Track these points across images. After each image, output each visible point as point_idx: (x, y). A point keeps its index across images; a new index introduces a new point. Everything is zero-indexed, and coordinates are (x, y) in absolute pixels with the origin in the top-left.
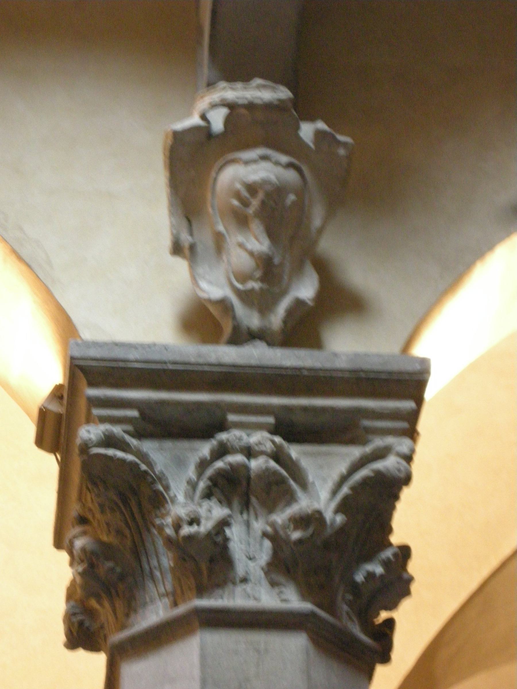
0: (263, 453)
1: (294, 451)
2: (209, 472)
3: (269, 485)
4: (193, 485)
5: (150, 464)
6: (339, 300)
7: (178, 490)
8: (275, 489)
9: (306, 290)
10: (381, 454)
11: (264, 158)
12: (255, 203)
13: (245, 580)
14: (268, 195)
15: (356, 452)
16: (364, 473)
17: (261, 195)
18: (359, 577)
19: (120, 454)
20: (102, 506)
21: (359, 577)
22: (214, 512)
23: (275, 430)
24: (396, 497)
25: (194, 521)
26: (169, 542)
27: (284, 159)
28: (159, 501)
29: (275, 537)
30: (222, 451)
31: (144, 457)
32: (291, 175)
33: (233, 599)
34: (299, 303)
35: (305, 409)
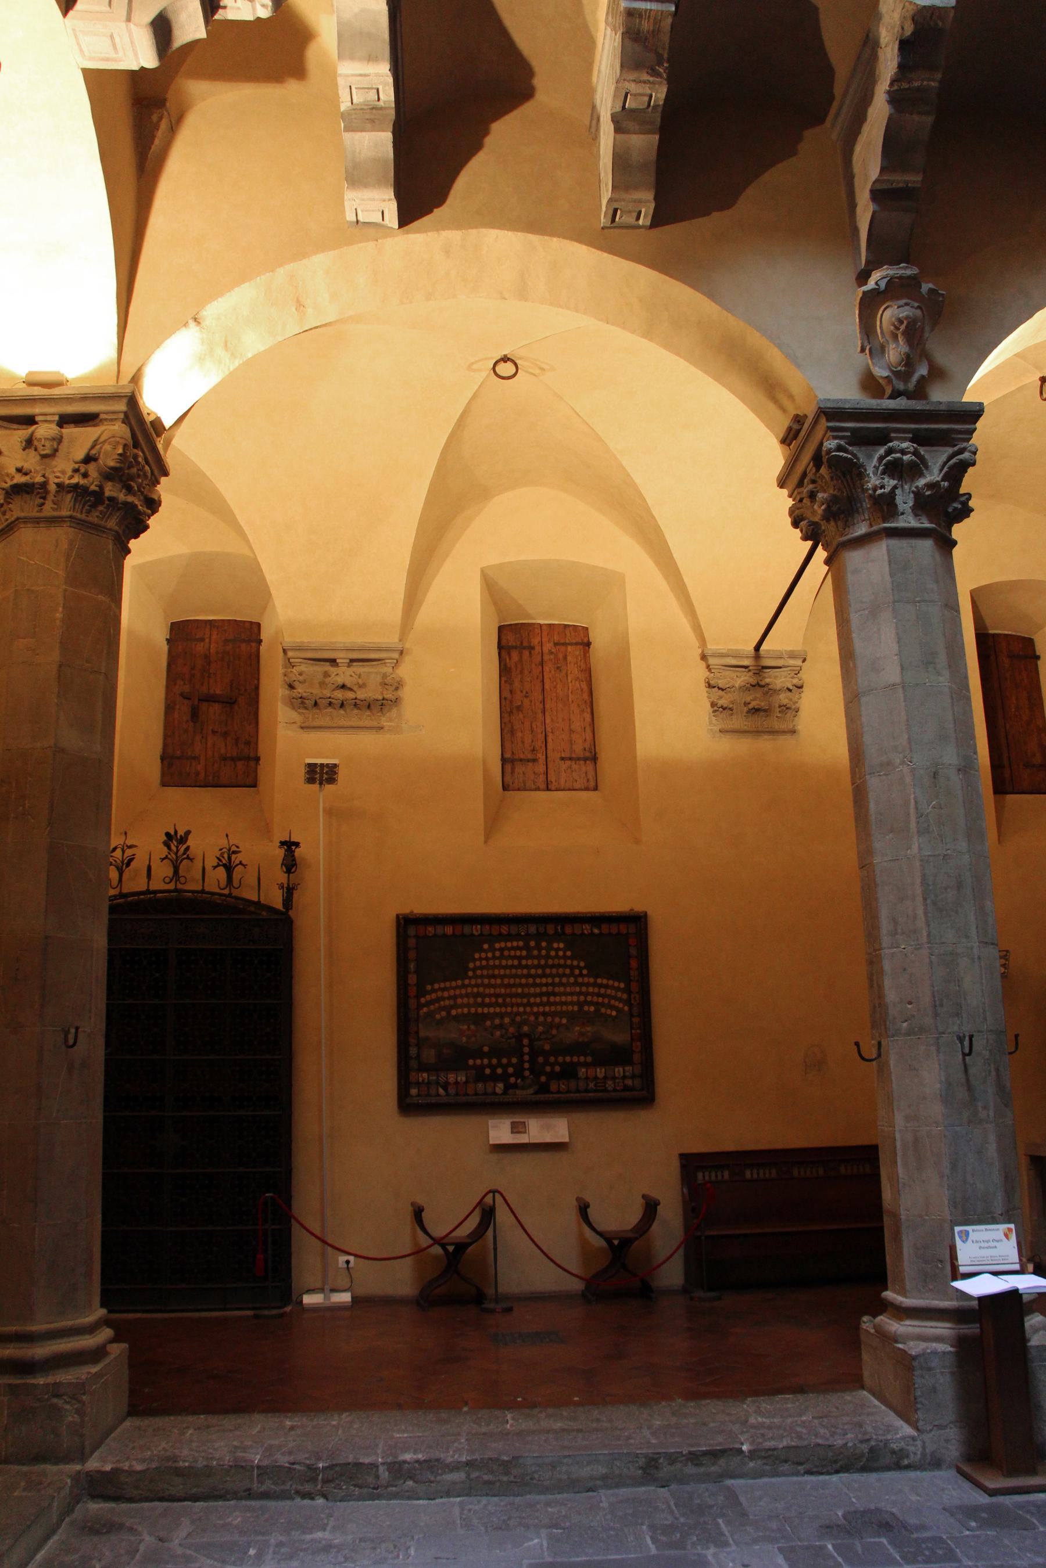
0: (909, 453)
1: (922, 451)
2: (884, 462)
4: (876, 468)
5: (858, 459)
6: (937, 373)
7: (870, 471)
8: (916, 469)
9: (923, 370)
10: (962, 451)
11: (907, 304)
12: (903, 327)
13: (903, 514)
14: (909, 323)
15: (950, 450)
18: (950, 510)
19: (845, 455)
20: (832, 478)
21: (950, 510)
23: (912, 440)
25: (882, 487)
26: (870, 496)
27: (916, 304)
29: (918, 494)
32: (918, 312)
33: (901, 523)
34: (923, 377)
35: (926, 430)
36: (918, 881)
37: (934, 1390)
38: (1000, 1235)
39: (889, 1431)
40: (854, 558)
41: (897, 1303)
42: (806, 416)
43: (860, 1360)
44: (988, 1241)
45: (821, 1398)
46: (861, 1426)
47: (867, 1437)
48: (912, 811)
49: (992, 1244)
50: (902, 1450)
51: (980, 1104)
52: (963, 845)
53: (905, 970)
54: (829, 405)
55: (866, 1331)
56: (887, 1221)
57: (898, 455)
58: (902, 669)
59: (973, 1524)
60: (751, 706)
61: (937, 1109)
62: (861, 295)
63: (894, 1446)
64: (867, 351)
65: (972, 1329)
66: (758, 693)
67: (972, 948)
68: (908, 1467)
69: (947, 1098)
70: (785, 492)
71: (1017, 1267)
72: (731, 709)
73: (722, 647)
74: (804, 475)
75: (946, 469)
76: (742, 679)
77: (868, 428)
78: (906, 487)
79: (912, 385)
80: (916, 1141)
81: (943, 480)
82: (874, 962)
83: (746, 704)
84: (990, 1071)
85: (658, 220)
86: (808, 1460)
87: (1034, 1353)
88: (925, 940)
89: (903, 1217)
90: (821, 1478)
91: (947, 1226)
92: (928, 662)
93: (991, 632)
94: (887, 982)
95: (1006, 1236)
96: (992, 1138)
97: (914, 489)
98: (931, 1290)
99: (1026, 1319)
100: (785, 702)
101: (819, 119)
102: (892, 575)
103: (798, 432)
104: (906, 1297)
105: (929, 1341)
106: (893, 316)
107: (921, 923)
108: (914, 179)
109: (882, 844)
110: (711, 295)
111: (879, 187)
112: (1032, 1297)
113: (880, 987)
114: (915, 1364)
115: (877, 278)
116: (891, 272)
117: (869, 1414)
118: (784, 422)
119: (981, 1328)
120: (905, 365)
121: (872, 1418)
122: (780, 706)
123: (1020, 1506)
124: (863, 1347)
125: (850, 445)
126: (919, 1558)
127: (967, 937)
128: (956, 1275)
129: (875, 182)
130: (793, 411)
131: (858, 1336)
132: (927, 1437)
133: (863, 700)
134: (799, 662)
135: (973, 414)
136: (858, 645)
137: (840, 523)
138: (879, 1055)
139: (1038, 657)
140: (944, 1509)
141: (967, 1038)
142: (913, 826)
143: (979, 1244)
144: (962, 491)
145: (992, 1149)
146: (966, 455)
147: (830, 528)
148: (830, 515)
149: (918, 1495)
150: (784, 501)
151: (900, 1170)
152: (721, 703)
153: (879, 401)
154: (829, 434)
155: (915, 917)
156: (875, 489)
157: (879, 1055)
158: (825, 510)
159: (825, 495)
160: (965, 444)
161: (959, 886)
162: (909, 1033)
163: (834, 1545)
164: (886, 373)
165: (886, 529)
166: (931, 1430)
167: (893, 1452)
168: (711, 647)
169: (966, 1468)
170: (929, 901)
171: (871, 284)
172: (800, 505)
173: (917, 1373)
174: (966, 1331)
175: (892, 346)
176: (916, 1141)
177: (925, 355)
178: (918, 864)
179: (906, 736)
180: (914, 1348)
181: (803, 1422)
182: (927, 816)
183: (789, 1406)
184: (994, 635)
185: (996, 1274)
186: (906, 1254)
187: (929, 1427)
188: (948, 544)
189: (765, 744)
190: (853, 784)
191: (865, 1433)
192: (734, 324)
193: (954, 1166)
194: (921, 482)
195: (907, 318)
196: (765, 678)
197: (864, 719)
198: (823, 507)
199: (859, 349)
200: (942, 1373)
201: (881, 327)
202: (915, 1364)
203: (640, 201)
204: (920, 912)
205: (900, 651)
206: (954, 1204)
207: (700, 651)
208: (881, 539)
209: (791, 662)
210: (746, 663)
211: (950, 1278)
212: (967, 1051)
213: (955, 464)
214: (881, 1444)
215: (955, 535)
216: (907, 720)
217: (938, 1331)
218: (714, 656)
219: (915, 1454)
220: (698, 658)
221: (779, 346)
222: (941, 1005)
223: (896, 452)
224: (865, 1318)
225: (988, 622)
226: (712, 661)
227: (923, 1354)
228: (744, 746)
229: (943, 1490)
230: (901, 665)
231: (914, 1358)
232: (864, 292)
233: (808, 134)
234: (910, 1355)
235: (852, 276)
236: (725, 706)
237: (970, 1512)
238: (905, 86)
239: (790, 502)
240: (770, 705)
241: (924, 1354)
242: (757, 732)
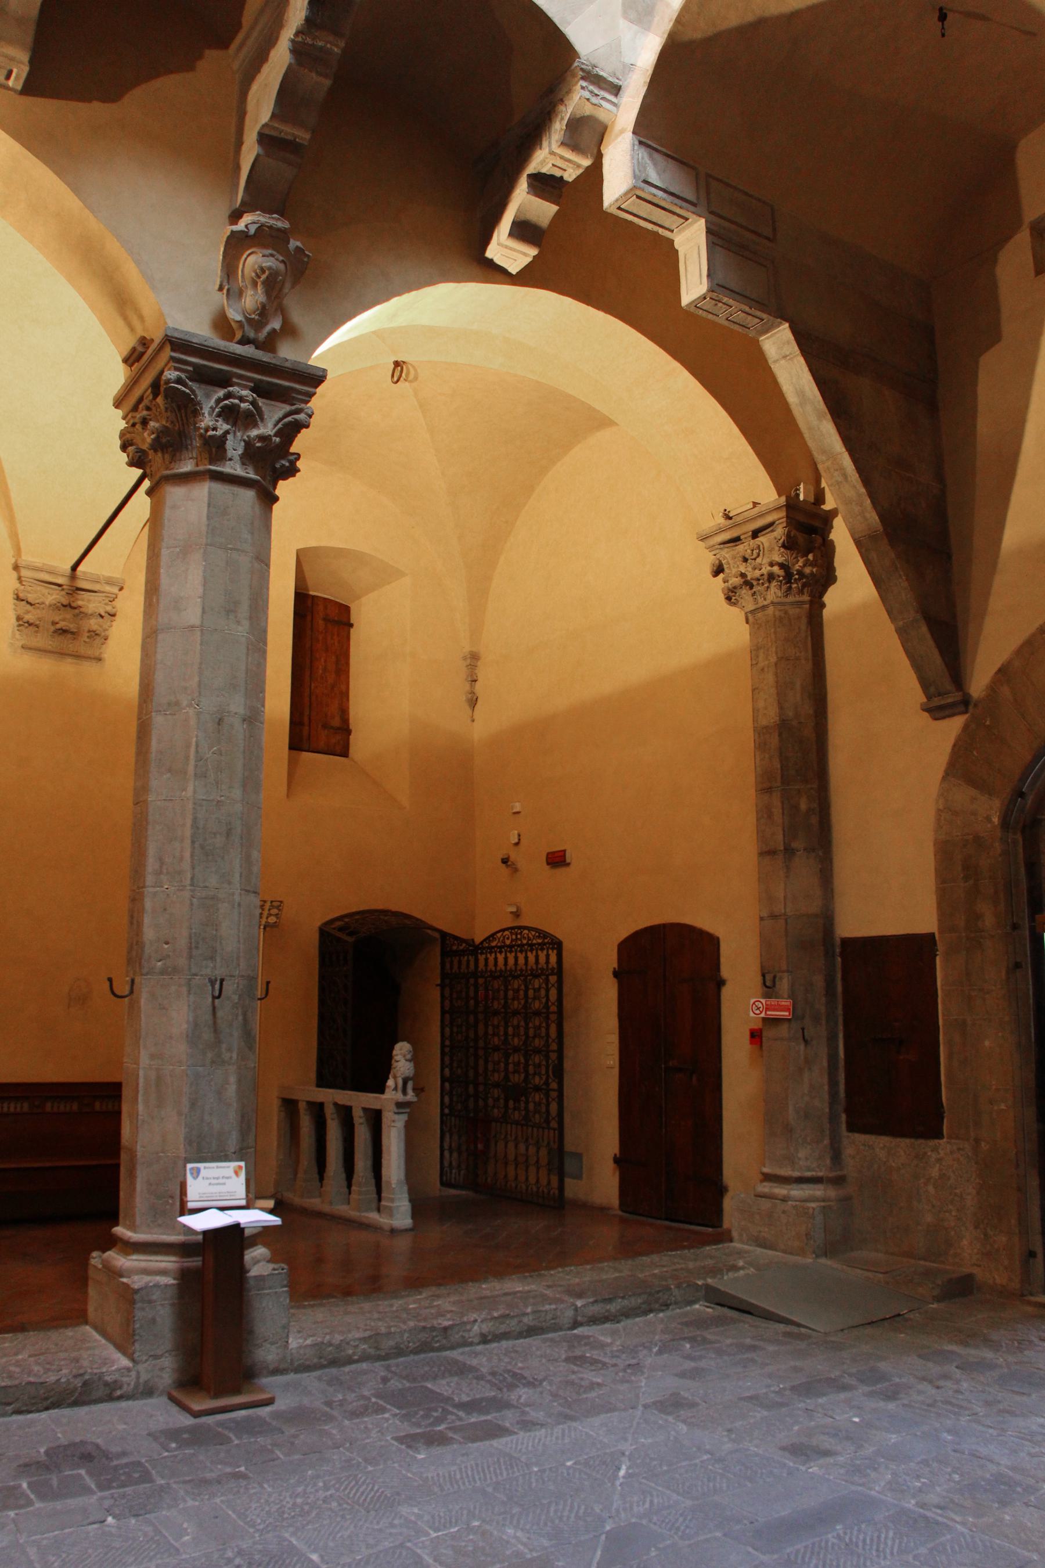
0: (247, 401)
1: (261, 402)
2: (221, 404)
3: (247, 416)
4: (213, 409)
5: (196, 395)
6: (289, 330)
7: (206, 411)
8: (251, 419)
9: (276, 324)
10: (298, 411)
11: (272, 255)
12: (264, 277)
13: (230, 460)
14: (270, 274)
15: (287, 408)
16: (289, 419)
17: (267, 273)
20: (166, 409)
21: (278, 466)
22: (223, 426)
23: (253, 390)
24: (299, 432)
25: (215, 429)
26: (201, 435)
27: (281, 258)
28: (196, 413)
29: (248, 444)
30: (229, 396)
31: (193, 391)
32: (282, 267)
33: (227, 468)
34: (274, 330)
35: (269, 383)
36: (189, 822)
37: (153, 1321)
38: (230, 1172)
39: (105, 1364)
40: (175, 493)
41: (126, 1238)
42: (152, 340)
43: (86, 1292)
44: (218, 1178)
45: (42, 1334)
46: (77, 1361)
47: (81, 1371)
48: (193, 749)
49: (221, 1181)
50: (115, 1381)
51: (224, 1046)
52: (237, 793)
53: (165, 910)
54: (176, 335)
55: (95, 1266)
56: (124, 1157)
57: (237, 401)
58: (204, 612)
59: (174, 1445)
60: (58, 626)
61: (181, 1049)
62: (228, 233)
63: (108, 1378)
64: (225, 291)
65: (195, 1262)
66: (69, 614)
67: (233, 894)
68: (120, 1398)
69: (193, 1038)
70: (120, 413)
71: (243, 1203)
72: (37, 626)
73: (38, 561)
74: (141, 399)
75: (280, 426)
76: (53, 597)
77: (212, 368)
78: (239, 434)
79: (262, 335)
80: (159, 1079)
81: (276, 435)
82: (136, 898)
83: (54, 623)
84: (237, 1015)
85: (29, 88)
86: (17, 1399)
87: (252, 1282)
88: (188, 882)
89: (139, 1154)
90: (30, 1416)
91: (181, 1163)
92: (230, 610)
93: (311, 593)
94: (147, 920)
95: (236, 1173)
96: (233, 1079)
97: (245, 438)
98: (160, 1225)
99: (246, 1252)
100: (95, 627)
101: (224, 44)
102: (209, 518)
103: (142, 354)
104: (135, 1232)
105: (150, 1274)
106: (256, 263)
107: (186, 865)
108: (303, 136)
109: (159, 783)
110: (76, 190)
111: (267, 131)
112: (255, 1231)
113: (140, 925)
114: (137, 1297)
115: (248, 221)
116: (263, 219)
117: (88, 1349)
118: (130, 342)
119: (203, 1261)
120: (260, 315)
121: (89, 1352)
122: (89, 631)
123: (220, 1424)
124: (90, 1283)
125: (191, 380)
126: (114, 1484)
127: (230, 883)
128: (184, 1211)
129: (263, 126)
130: (140, 332)
131: (86, 1271)
132: (141, 1367)
133: (160, 637)
134: (115, 590)
135: (315, 378)
136: (164, 581)
137: (167, 456)
138: (132, 992)
139: (351, 625)
140: (149, 1434)
141: (218, 982)
142: (191, 768)
143: (208, 1181)
144: (292, 450)
145: (232, 1090)
146: (302, 416)
147: (157, 459)
148: (158, 445)
149: (125, 1423)
150: (116, 422)
151: (141, 1107)
152: (27, 617)
153: (227, 344)
154: (172, 364)
155: (181, 859)
156: (207, 430)
157: (132, 992)
158: (154, 440)
159: (157, 425)
160: (303, 406)
161: (229, 833)
162: (163, 972)
163: (29, 1484)
164: (239, 318)
165: (210, 471)
166: (146, 1360)
167: (106, 1384)
168: (26, 558)
169: (175, 1393)
170: (197, 845)
171: (241, 226)
172: (131, 429)
173: (138, 1305)
174: (190, 1264)
175: (250, 292)
176: (159, 1079)
177: (282, 310)
178: (191, 806)
179: (196, 679)
180: (137, 1282)
181: (17, 1361)
182: (206, 760)
183: (6, 1345)
184: (314, 597)
185: (222, 1209)
186: (138, 1192)
187: (145, 1358)
188: (269, 499)
189: (67, 668)
190: (139, 719)
191: (81, 1367)
192: (94, 225)
193: (193, 1104)
194: (254, 433)
195: (270, 268)
196: (77, 599)
197: (159, 657)
198: (153, 436)
199: (217, 287)
200: (162, 1305)
201: (243, 271)
202: (137, 1297)
203: (12, 59)
204: (187, 854)
205: (204, 594)
206: (189, 1142)
207: (13, 561)
208: (204, 480)
209: (108, 588)
210: (60, 581)
211: (178, 1213)
212: (217, 993)
213: (290, 422)
214: (96, 1378)
215: (277, 492)
216: (201, 664)
217: (163, 1265)
218: (28, 568)
219: (129, 1384)
220: (10, 567)
221: (138, 263)
222: (197, 948)
223: (235, 397)
224: (95, 1254)
225: (310, 583)
226: (24, 573)
227: (146, 1287)
228: (44, 667)
229: (151, 1416)
230: (203, 608)
231: (136, 1291)
232: (232, 232)
233: (211, 54)
234: (133, 1289)
235: (223, 211)
236: (31, 621)
237: (173, 1434)
238: (309, 41)
239: (123, 424)
240: (78, 628)
241: (146, 1287)
242: (62, 654)
